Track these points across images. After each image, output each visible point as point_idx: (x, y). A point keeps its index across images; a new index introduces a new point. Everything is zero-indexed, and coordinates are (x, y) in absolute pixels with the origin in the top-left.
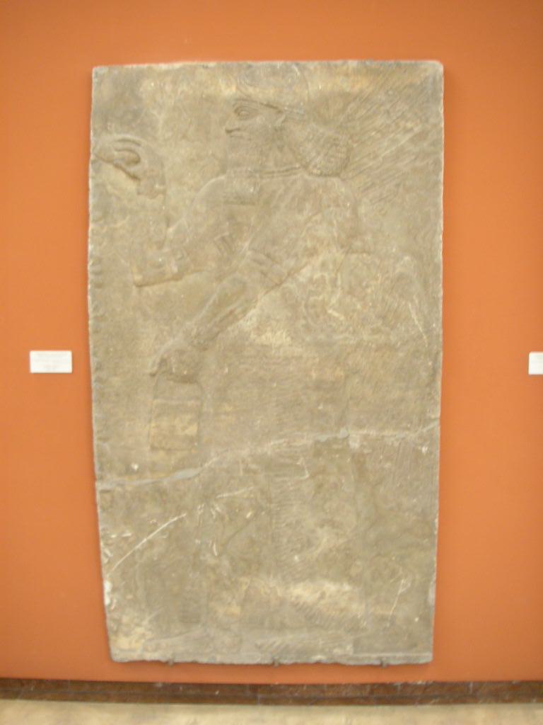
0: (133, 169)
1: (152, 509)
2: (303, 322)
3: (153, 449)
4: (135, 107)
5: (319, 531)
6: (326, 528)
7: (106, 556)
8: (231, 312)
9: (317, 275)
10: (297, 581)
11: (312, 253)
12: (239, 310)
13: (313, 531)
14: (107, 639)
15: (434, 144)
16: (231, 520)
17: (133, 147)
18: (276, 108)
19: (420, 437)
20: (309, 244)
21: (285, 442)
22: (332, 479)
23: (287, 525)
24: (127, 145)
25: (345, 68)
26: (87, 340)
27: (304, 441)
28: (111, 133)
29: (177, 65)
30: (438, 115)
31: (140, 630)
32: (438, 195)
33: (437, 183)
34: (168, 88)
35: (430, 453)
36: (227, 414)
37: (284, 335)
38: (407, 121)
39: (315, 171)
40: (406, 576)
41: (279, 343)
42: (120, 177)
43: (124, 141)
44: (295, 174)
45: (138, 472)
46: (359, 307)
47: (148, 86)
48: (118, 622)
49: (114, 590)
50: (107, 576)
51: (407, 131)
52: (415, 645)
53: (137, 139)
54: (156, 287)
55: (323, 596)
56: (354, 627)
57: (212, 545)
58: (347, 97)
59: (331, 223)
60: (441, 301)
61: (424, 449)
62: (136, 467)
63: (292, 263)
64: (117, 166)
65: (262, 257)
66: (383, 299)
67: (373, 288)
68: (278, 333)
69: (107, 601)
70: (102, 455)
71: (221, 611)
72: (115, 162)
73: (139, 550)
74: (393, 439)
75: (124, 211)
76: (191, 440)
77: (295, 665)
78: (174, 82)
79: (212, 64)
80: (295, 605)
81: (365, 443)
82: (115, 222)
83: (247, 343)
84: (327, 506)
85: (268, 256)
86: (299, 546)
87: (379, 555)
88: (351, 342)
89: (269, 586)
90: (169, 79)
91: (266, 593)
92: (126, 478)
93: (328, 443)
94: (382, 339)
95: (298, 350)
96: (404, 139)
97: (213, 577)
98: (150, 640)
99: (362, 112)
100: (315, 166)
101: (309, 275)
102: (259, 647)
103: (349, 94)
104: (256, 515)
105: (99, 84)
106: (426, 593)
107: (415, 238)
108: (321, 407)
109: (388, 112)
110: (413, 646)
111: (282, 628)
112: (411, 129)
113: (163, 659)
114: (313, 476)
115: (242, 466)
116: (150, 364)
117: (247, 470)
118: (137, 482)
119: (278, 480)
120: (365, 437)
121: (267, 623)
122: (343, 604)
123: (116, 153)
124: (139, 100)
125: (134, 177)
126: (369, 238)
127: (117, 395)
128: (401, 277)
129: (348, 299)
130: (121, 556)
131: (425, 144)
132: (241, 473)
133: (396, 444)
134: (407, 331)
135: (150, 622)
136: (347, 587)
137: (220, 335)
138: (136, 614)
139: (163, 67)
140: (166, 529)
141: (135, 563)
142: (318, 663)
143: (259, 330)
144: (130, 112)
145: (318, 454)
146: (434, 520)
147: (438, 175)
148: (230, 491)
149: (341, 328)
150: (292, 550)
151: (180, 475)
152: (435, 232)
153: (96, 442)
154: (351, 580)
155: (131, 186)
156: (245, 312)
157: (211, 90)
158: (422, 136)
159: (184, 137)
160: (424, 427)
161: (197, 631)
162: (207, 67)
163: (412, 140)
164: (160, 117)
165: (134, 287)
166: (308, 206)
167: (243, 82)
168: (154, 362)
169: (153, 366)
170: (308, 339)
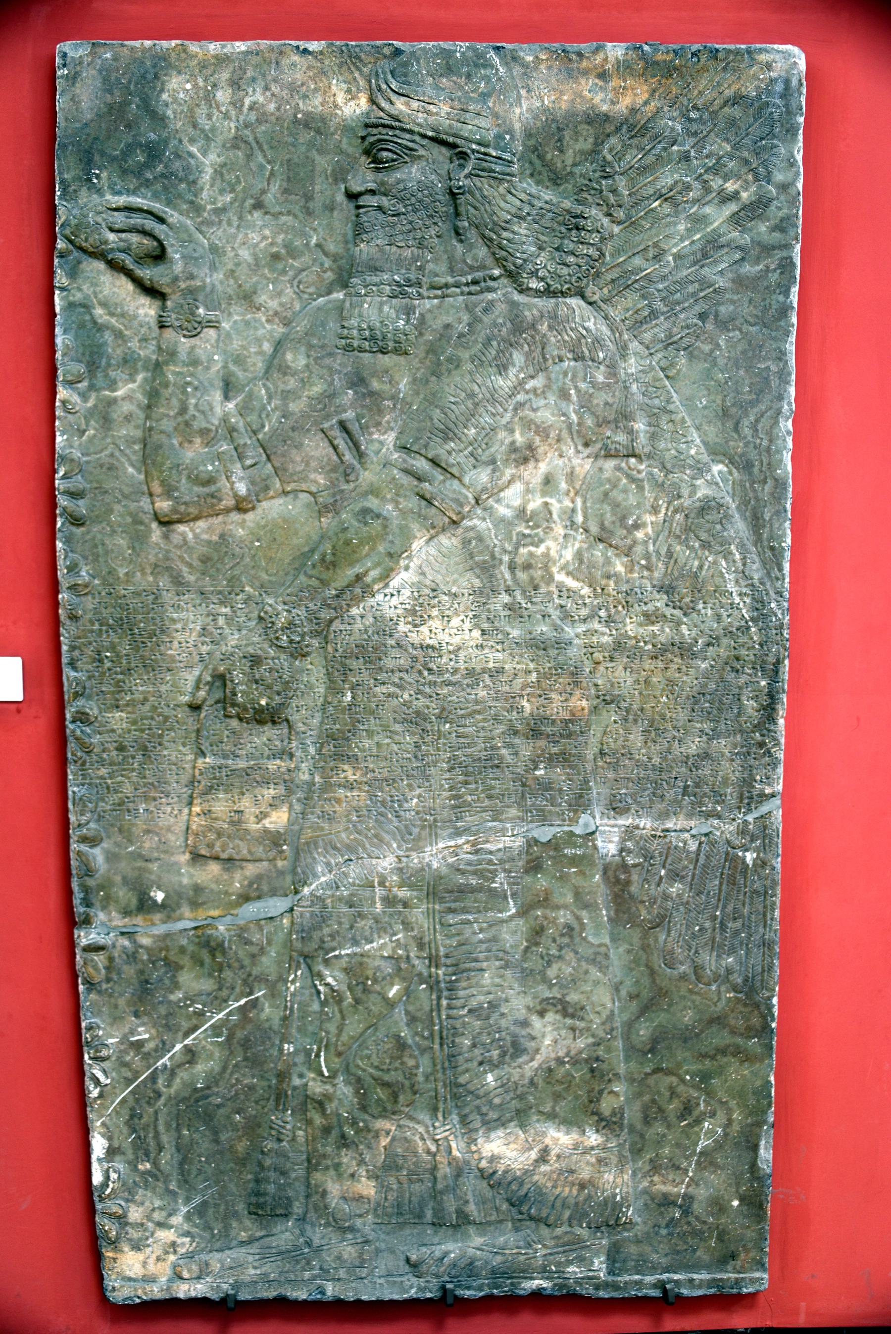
0: (146, 273)
1: (192, 981)
2: (505, 598)
3: (197, 858)
4: (152, 136)
5: (537, 1022)
6: (550, 1017)
7: (97, 1082)
8: (359, 578)
9: (535, 504)
10: (490, 1125)
11: (525, 456)
12: (374, 573)
13: (525, 1024)
14: (97, 1257)
15: (781, 227)
16: (357, 1001)
17: (150, 224)
18: (453, 146)
19: (743, 831)
20: (519, 438)
21: (467, 842)
22: (563, 917)
23: (470, 1011)
24: (137, 220)
25: (599, 58)
26: (57, 635)
27: (506, 841)
28: (99, 192)
29: (241, 46)
30: (792, 164)
31: (166, 1236)
32: (787, 334)
33: (784, 311)
34: (223, 96)
35: (761, 863)
36: (349, 786)
37: (467, 625)
38: (726, 179)
39: (534, 284)
40: (713, 1115)
41: (456, 640)
42: (121, 289)
43: (129, 209)
44: (489, 290)
45: (164, 906)
46: (620, 568)
47: (178, 88)
48: (121, 1219)
49: (111, 1152)
50: (96, 1123)
51: (726, 198)
52: (733, 1257)
53: (157, 206)
54: (201, 524)
55: (543, 1157)
56: (609, 1218)
57: (318, 1056)
58: (599, 123)
59: (564, 395)
60: (788, 555)
61: (750, 857)
62: (160, 896)
63: (483, 476)
64: (114, 266)
65: (421, 465)
66: (670, 554)
67: (649, 530)
68: (455, 622)
69: (97, 1178)
70: (89, 872)
71: (334, 1189)
72: (110, 257)
73: (165, 1066)
74: (687, 835)
75: (129, 362)
76: (275, 839)
77: (489, 1299)
78: (235, 84)
79: (314, 46)
80: (486, 1176)
81: (629, 844)
82: (113, 385)
83: (391, 642)
84: (551, 972)
85: (434, 462)
86: (495, 1053)
87: (657, 1070)
88: (606, 639)
89: (431, 1137)
90: (224, 76)
91: (428, 1152)
92: (139, 920)
93: (554, 845)
94: (663, 632)
95: (494, 657)
96: (718, 217)
97: (318, 1120)
98: (190, 1256)
99: (633, 158)
100: (534, 274)
101: (517, 503)
102: (414, 1266)
103: (606, 118)
104: (407, 992)
105: (73, 78)
106: (755, 1148)
107: (736, 429)
108: (540, 773)
109: (686, 157)
110: (727, 1258)
111: (462, 1223)
112: (735, 196)
113: (215, 1296)
114: (523, 912)
115: (379, 892)
116: (187, 681)
117: (389, 901)
118: (161, 929)
119: (451, 919)
120: (629, 832)
121: (429, 1215)
122: (585, 1174)
123: (112, 237)
124: (158, 119)
125: (151, 291)
126: (640, 426)
127: (121, 748)
128: (705, 507)
129: (599, 552)
130: (129, 1082)
131: (763, 228)
132: (379, 907)
133: (693, 846)
134: (718, 618)
135: (188, 1217)
136: (593, 1138)
137: (336, 625)
138: (157, 1203)
139: (213, 47)
140: (225, 1022)
141: (159, 1095)
142: (537, 1295)
143: (417, 614)
144: (139, 145)
145: (534, 866)
146: (770, 998)
147: (787, 293)
148: (355, 942)
149: (584, 612)
150: (481, 1063)
151: (251, 910)
152: (779, 412)
153: (74, 846)
154: (607, 1124)
155: (146, 310)
156: (386, 577)
157: (315, 105)
158: (756, 209)
159: (258, 205)
160: (749, 810)
161: (285, 1234)
162: (305, 51)
163: (736, 220)
164: (209, 161)
165: (154, 525)
166: (518, 357)
167: (384, 86)
168: (199, 681)
169: (197, 688)
170: (515, 633)
